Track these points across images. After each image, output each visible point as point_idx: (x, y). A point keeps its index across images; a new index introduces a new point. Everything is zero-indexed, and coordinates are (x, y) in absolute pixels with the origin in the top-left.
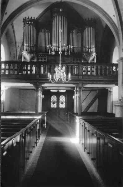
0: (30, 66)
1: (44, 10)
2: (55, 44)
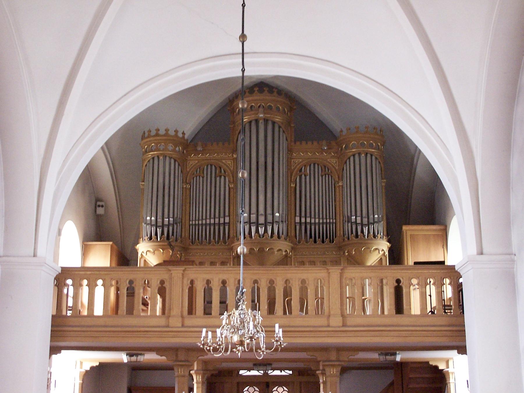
0: (103, 285)
1: (416, 178)
2: (148, 218)
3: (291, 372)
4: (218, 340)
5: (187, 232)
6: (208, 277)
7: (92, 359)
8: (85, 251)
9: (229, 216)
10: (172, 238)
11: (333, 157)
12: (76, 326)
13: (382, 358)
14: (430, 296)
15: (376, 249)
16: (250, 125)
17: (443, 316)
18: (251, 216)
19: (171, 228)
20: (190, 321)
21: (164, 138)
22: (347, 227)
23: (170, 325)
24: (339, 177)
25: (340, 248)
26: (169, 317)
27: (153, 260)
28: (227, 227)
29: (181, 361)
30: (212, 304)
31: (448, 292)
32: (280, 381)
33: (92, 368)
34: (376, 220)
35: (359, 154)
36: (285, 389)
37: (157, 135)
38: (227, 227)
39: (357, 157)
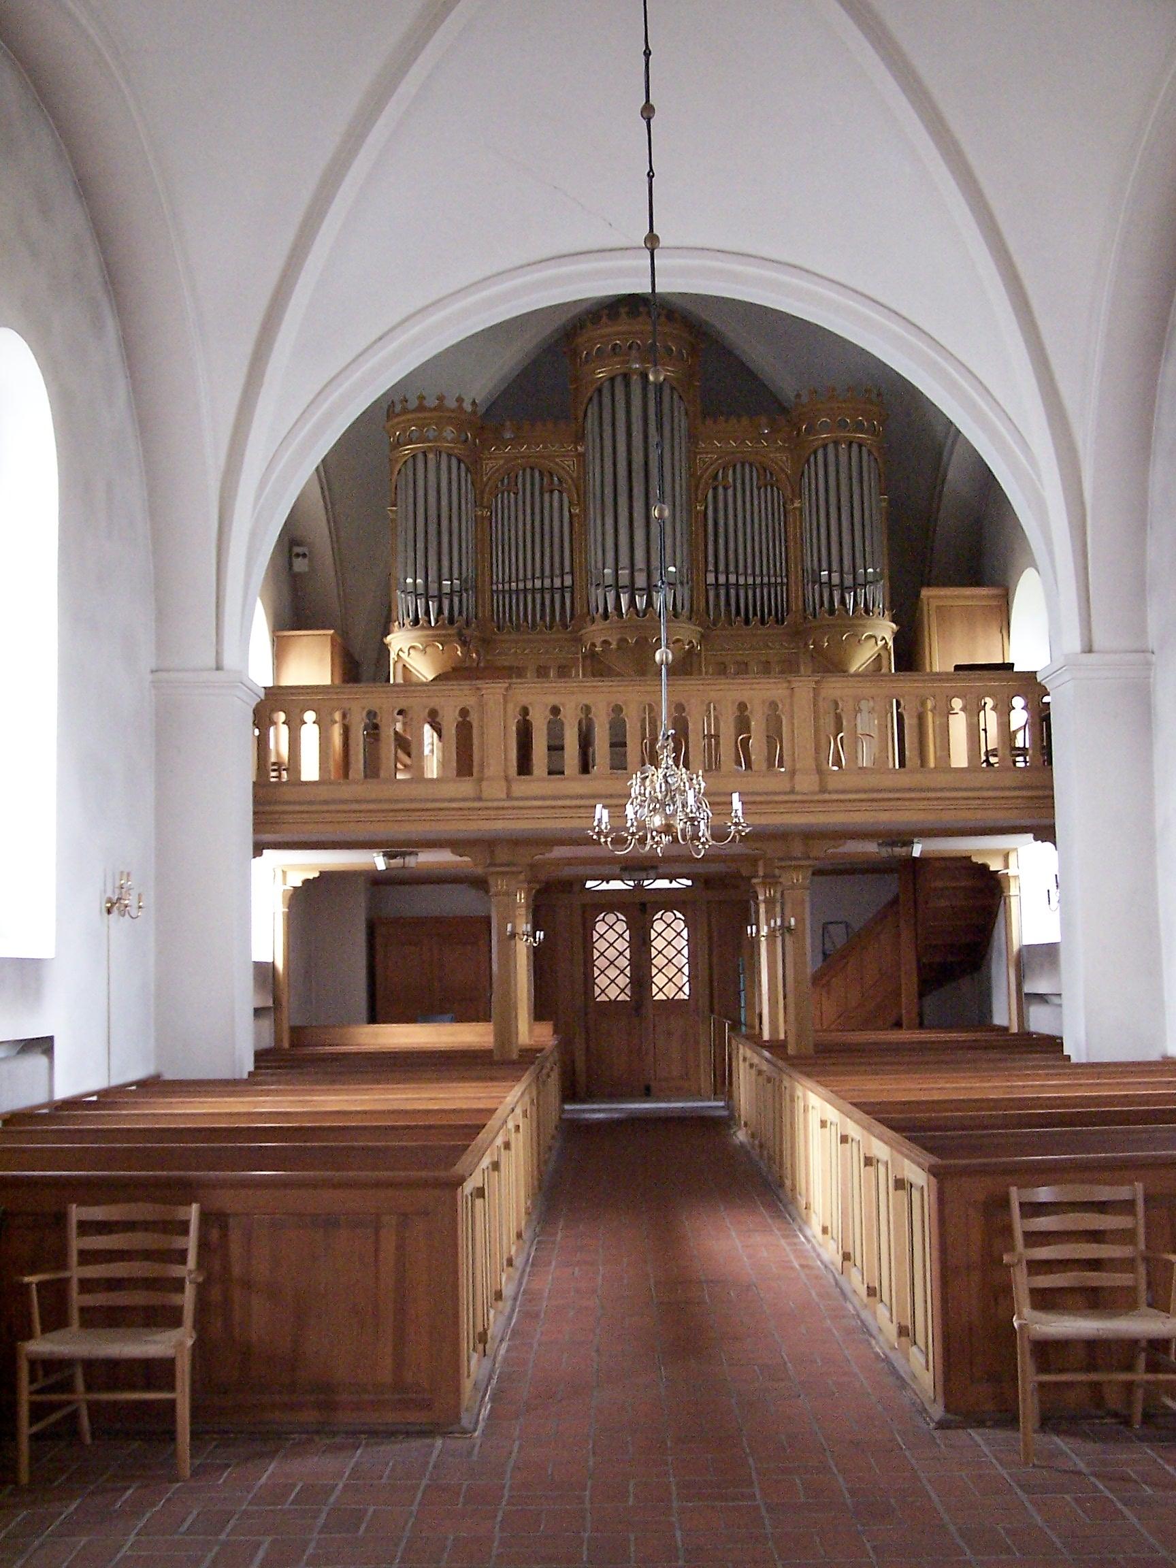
2: (409, 580)
3: (689, 883)
4: (629, 824)
5: (488, 607)
6: (552, 700)
7: (303, 865)
8: (280, 651)
9: (572, 573)
10: (460, 621)
11: (778, 449)
12: (295, 803)
13: (885, 852)
14: (985, 730)
15: (871, 637)
16: (613, 386)
17: (1008, 769)
18: (636, 574)
19: (456, 600)
20: (523, 787)
21: (436, 414)
22: (812, 592)
23: (485, 795)
24: (793, 491)
25: (798, 634)
26: (481, 780)
27: (424, 668)
28: (568, 595)
29: (501, 865)
30: (610, 751)
31: (1019, 717)
32: (668, 901)
33: (306, 882)
34: (870, 578)
35: (836, 443)
36: (679, 915)
37: (421, 408)
38: (568, 595)
39: (831, 448)
